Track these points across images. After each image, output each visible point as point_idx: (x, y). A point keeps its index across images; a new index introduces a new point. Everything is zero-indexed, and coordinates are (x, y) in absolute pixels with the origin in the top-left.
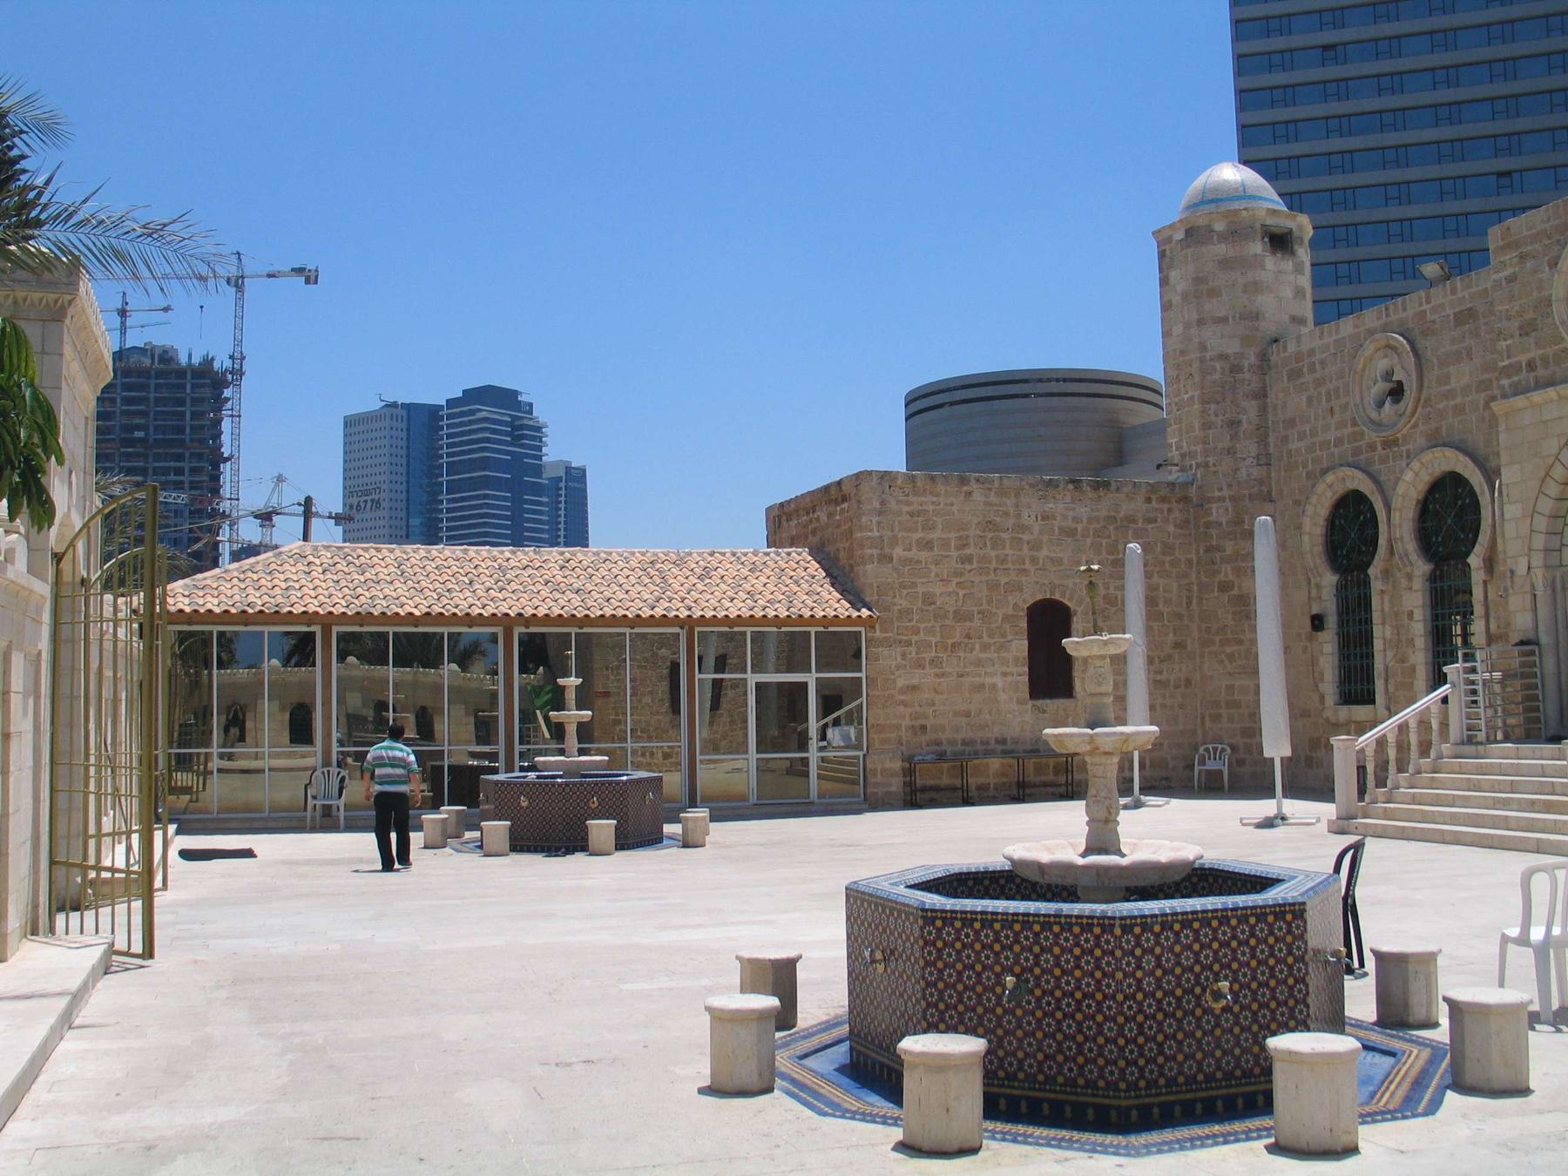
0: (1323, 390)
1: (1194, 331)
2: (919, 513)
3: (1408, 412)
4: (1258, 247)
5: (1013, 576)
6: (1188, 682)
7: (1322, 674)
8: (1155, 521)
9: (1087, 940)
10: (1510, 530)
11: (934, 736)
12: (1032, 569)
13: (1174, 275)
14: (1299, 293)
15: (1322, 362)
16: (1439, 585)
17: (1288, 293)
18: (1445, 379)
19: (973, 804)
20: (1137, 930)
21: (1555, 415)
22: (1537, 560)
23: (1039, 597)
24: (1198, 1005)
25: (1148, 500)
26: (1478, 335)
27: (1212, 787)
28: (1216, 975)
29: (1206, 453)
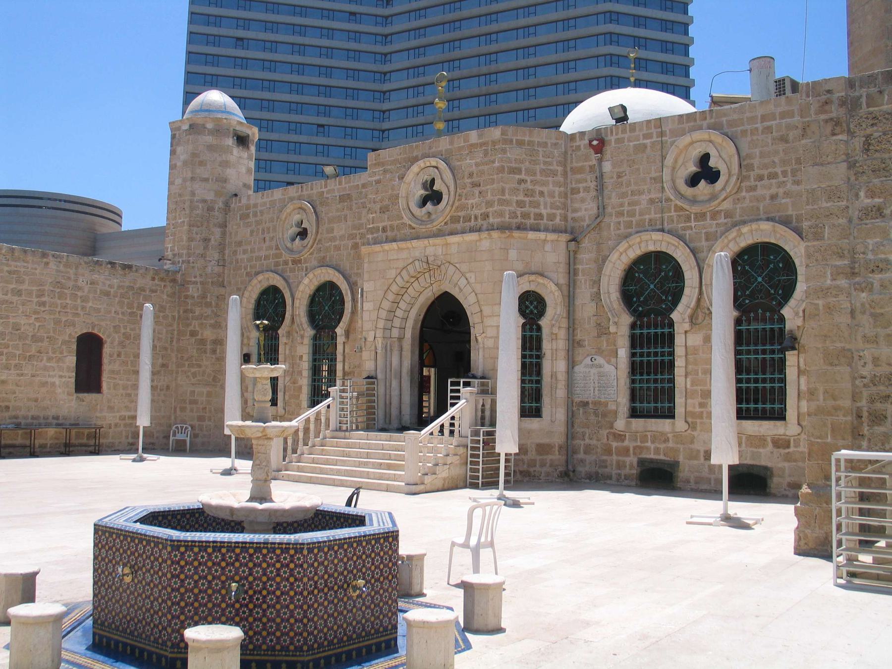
0: (260, 227)
1: (188, 184)
2: (14, 272)
3: (309, 246)
4: (230, 141)
5: (70, 317)
6: (168, 387)
7: (247, 388)
8: (156, 292)
9: (285, 558)
10: (366, 316)
11: (14, 413)
12: (82, 313)
13: (179, 149)
14: (249, 171)
15: (262, 212)
16: (318, 342)
17: (243, 170)
18: (331, 230)
19: (38, 456)
20: (316, 551)
21: (395, 257)
22: (379, 334)
23: (85, 331)
24: (345, 595)
25: (153, 279)
26: (351, 209)
27: (180, 450)
28: (355, 576)
29: (189, 255)
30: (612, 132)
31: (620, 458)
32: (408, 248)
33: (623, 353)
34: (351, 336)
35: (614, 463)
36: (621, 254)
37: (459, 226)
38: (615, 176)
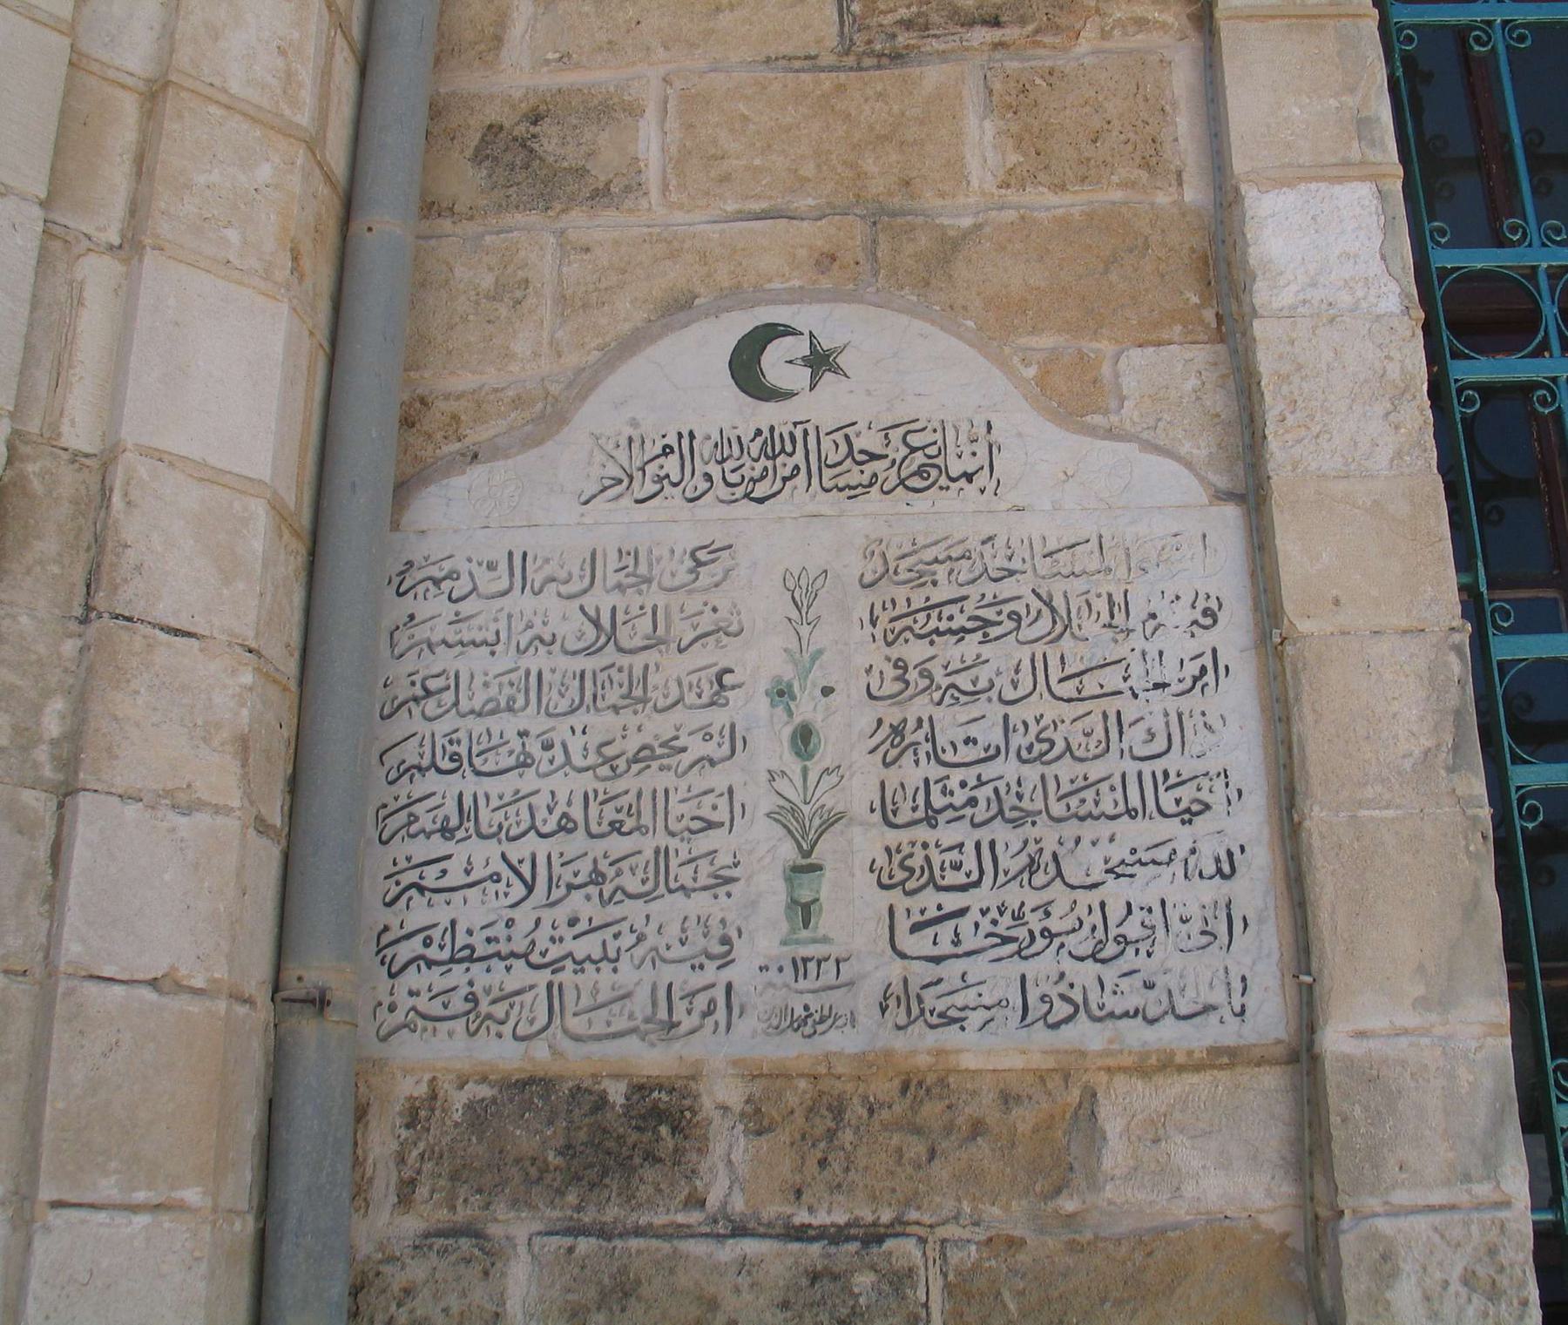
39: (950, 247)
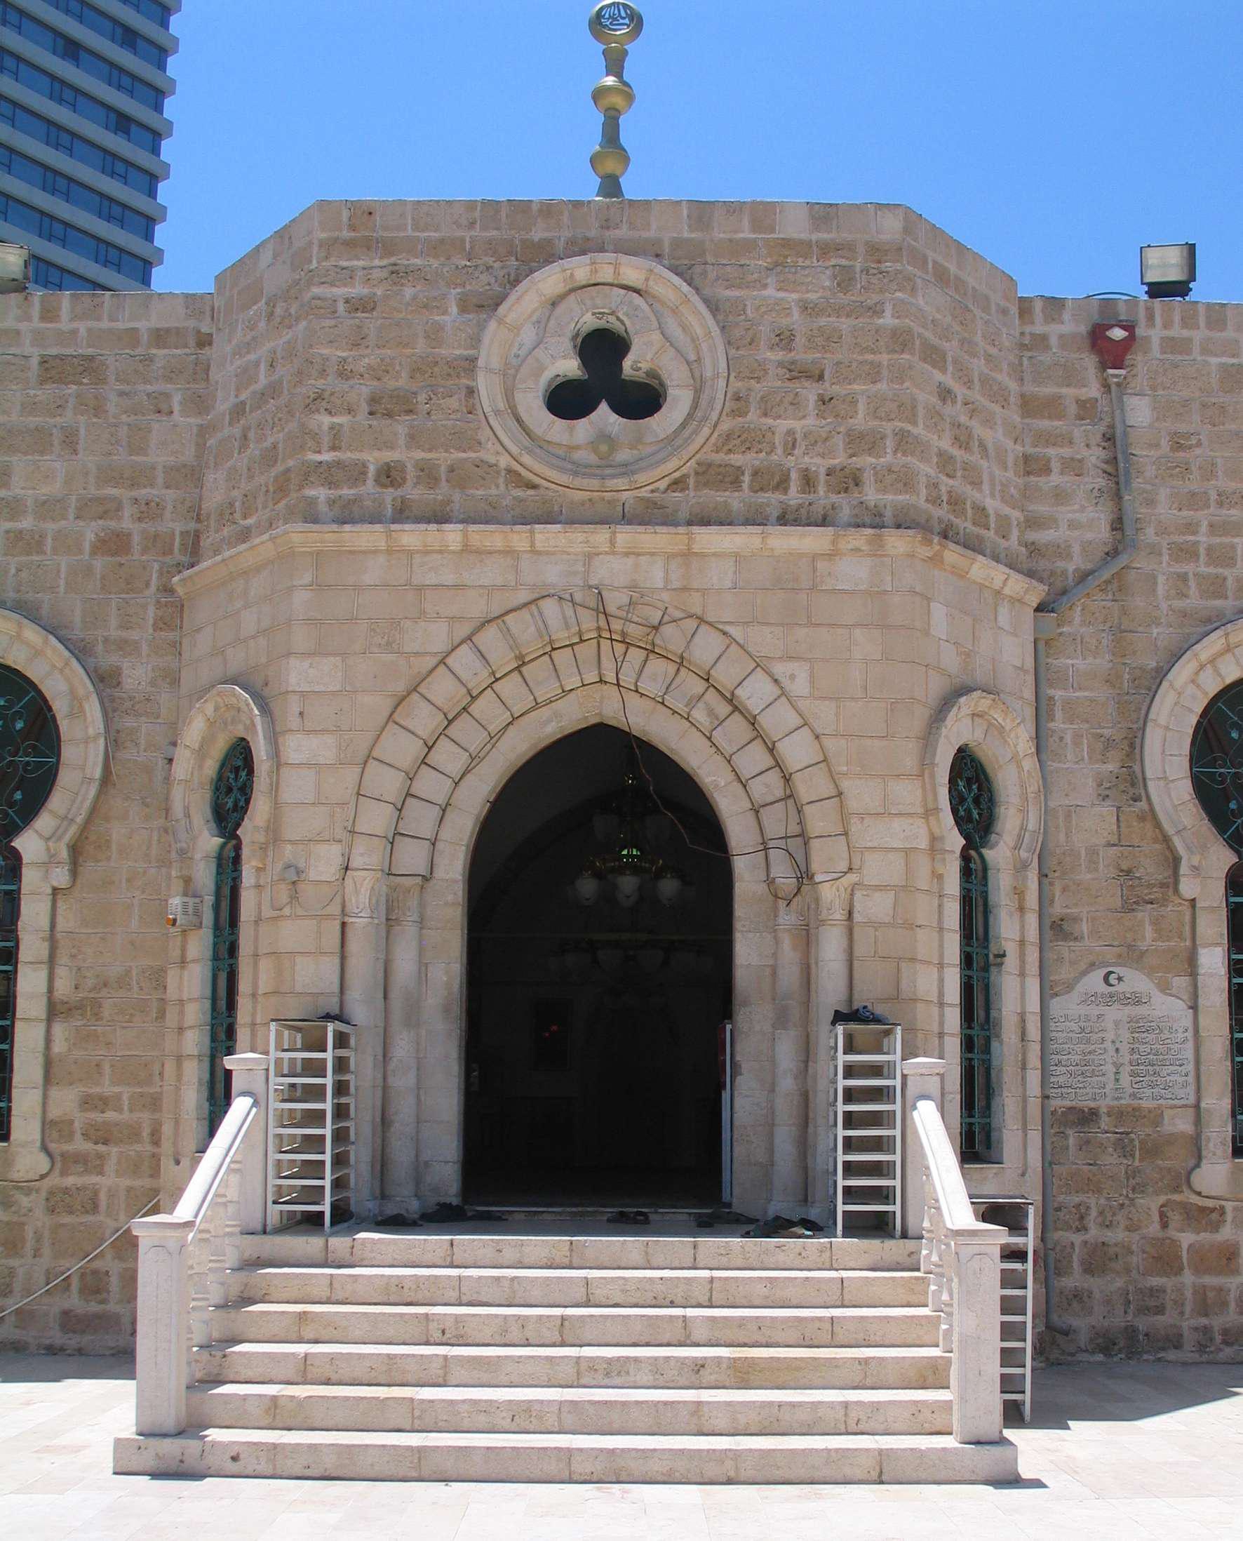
21: (449, 578)
22: (367, 856)
26: (99, 410)
30: (1150, 317)
31: (1210, 1280)
32: (509, 552)
33: (1214, 961)
34: (90, 870)
35: (1188, 1294)
36: (1202, 667)
37: (736, 501)
38: (1165, 443)
39: (1142, 954)
